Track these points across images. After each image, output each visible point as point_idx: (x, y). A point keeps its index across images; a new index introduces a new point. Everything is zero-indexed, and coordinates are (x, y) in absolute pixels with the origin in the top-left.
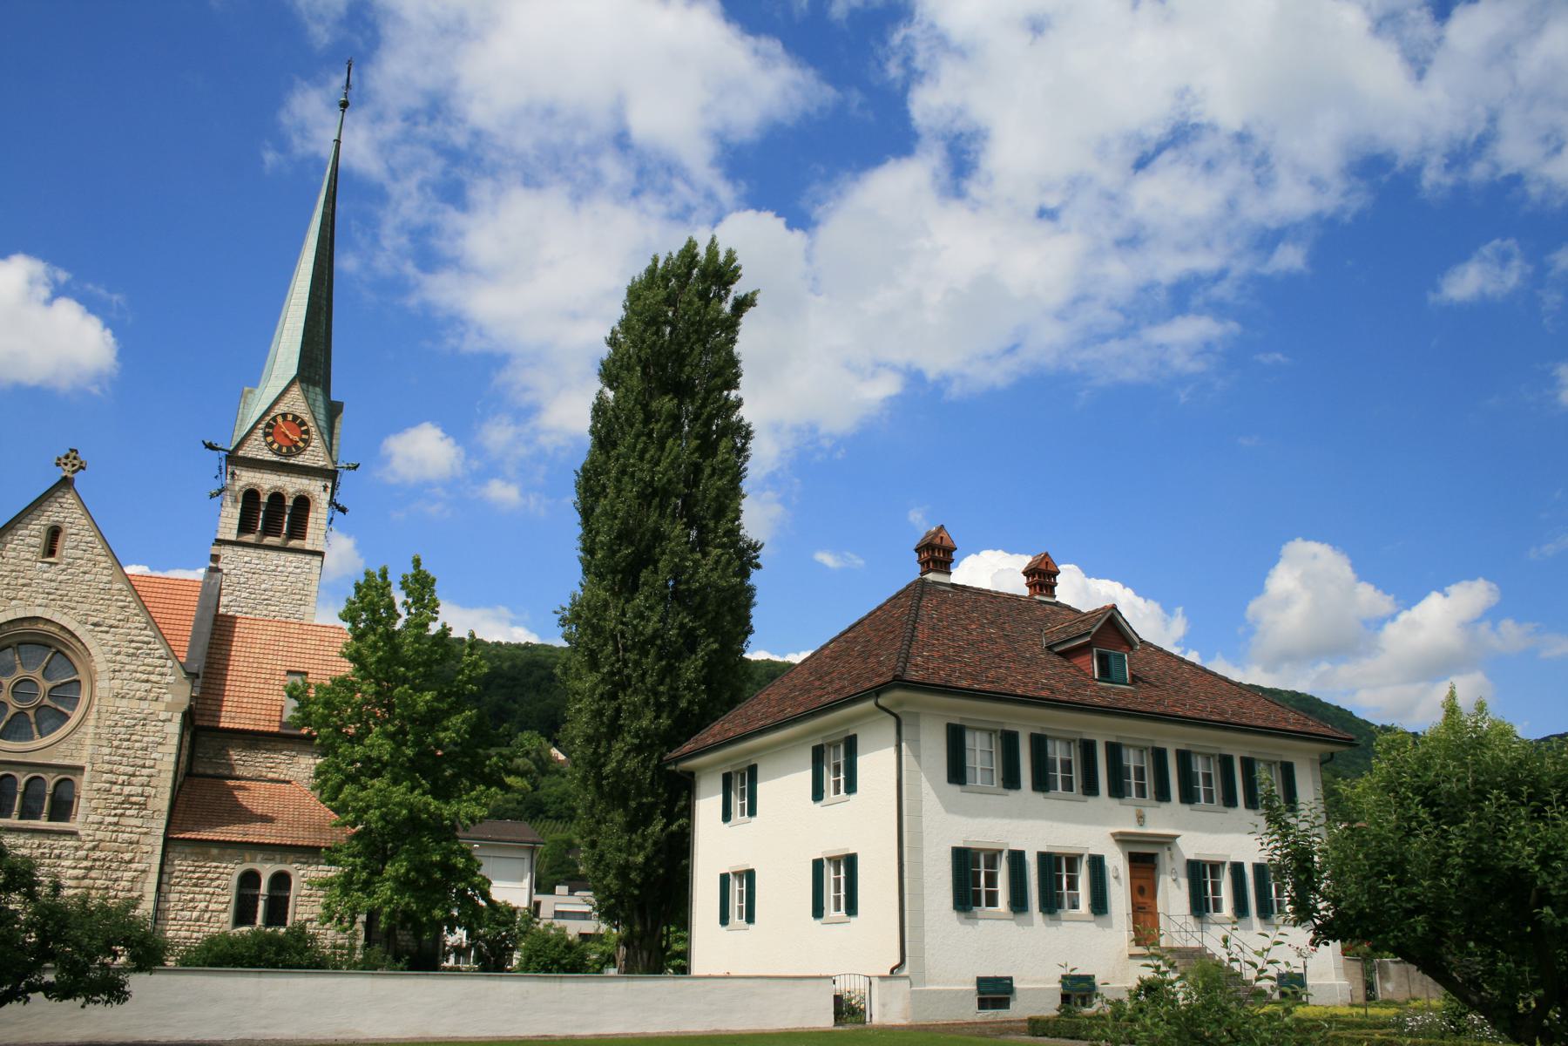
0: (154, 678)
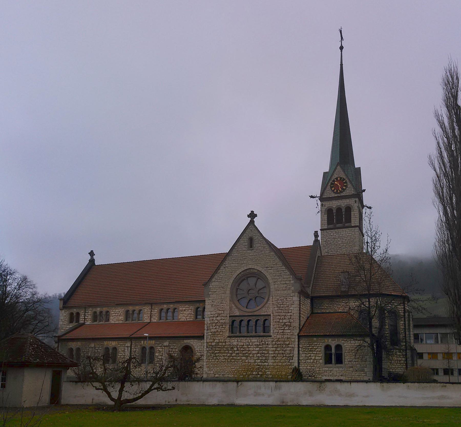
0: (287, 282)
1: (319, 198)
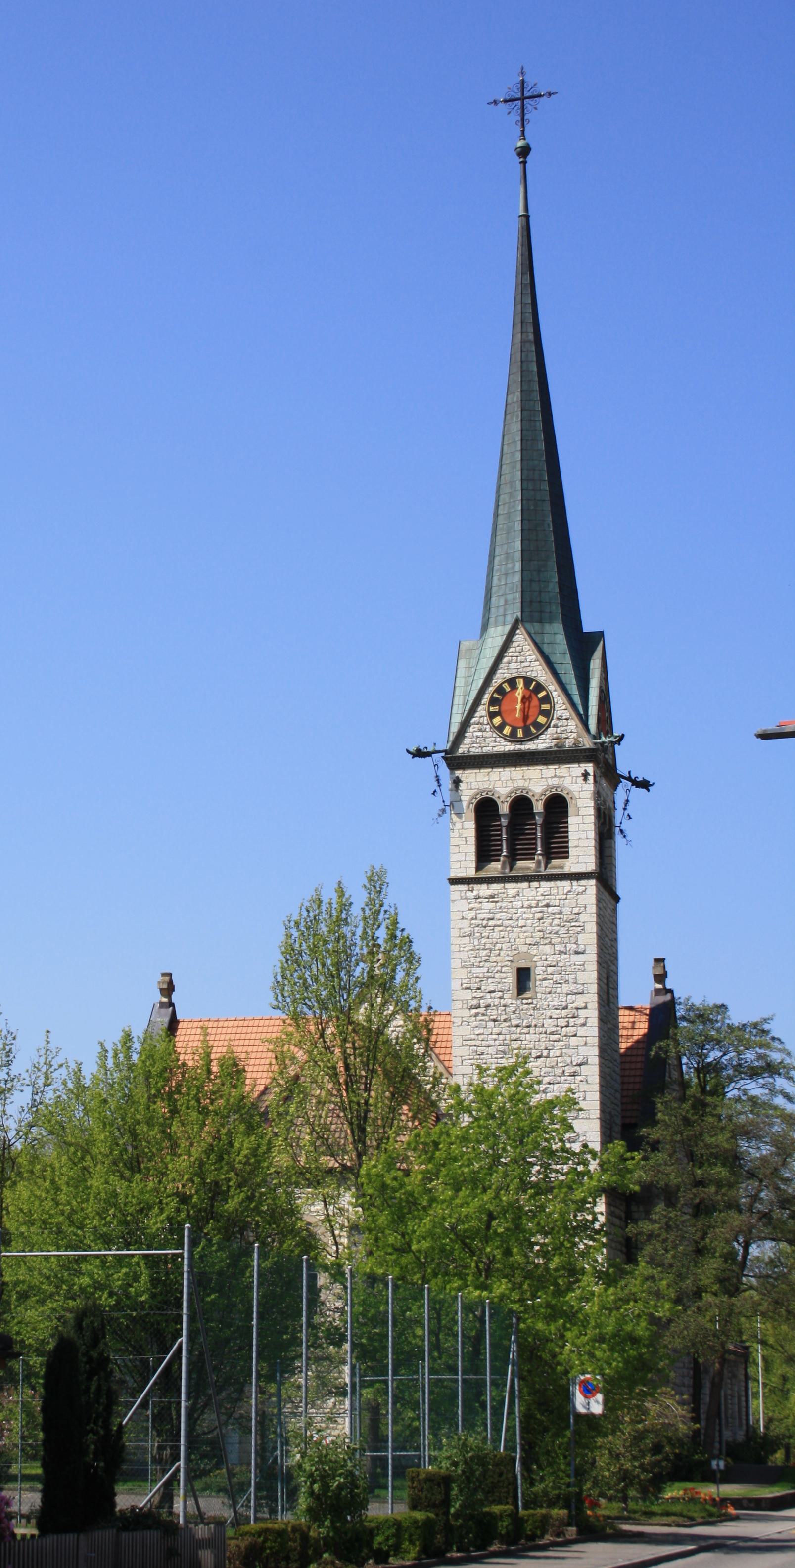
1: (443, 754)
